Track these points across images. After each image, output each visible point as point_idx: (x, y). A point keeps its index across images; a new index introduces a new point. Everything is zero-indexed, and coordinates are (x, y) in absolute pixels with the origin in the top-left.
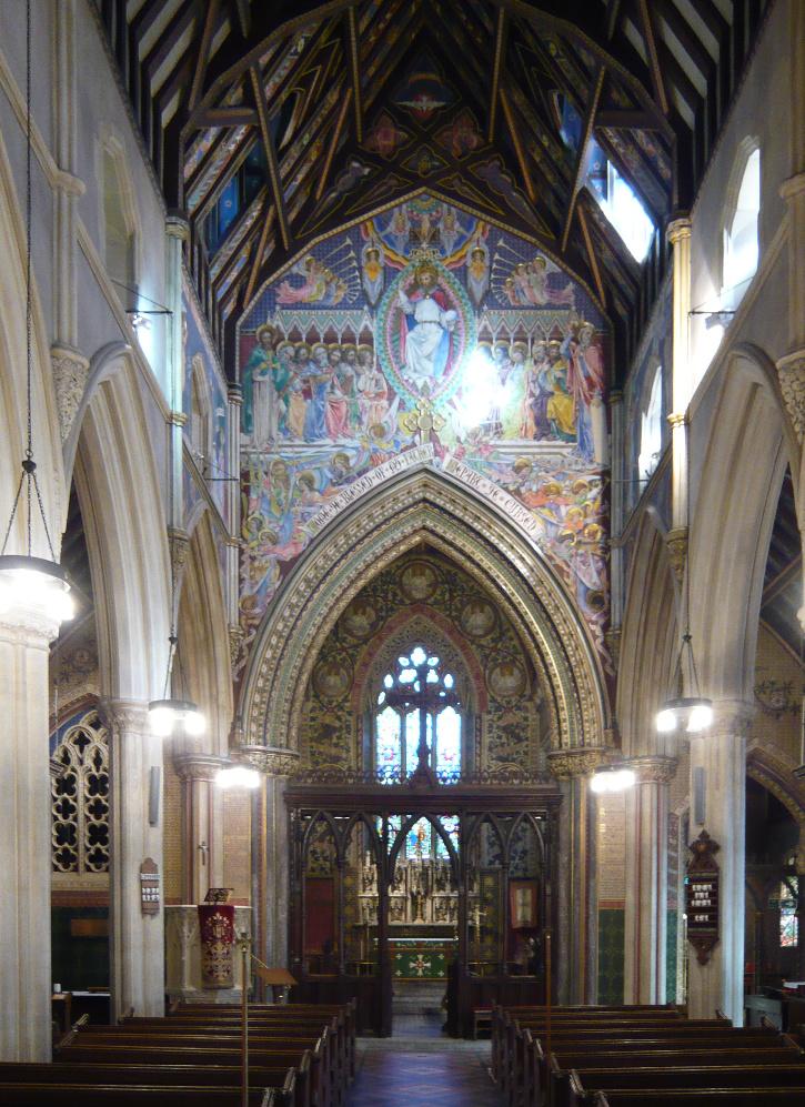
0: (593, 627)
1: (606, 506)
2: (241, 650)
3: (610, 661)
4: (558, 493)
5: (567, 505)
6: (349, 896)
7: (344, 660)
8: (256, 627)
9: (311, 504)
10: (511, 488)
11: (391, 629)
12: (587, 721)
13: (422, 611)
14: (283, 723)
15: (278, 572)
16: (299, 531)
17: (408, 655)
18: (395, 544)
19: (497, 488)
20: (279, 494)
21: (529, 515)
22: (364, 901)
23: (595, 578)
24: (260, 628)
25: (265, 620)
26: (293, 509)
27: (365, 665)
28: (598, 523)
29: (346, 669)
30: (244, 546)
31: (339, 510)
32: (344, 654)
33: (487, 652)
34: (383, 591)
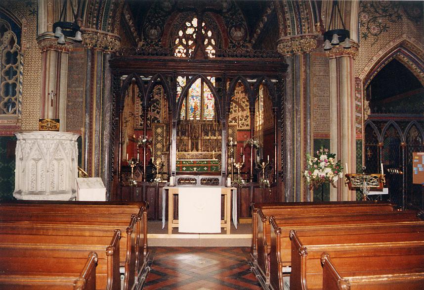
12: (303, 18)
29: (159, 26)
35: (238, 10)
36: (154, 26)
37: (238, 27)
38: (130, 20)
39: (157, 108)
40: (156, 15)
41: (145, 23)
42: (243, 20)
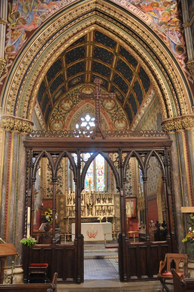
0: (180, 61)
1: (180, 11)
2: (4, 70)
3: (190, 75)
4: (158, 6)
5: (162, 11)
6: (62, 206)
7: (61, 118)
8: (13, 60)
9: (42, 9)
10: (136, 4)
11: (78, 108)
12: (182, 103)
13: (89, 102)
14: (25, 106)
15: (25, 36)
16: (36, 19)
17: (84, 117)
18: (83, 29)
19: (129, 4)
20: (27, 4)
21: (145, 15)
22: (68, 208)
23: (178, 40)
24: (15, 60)
25: (18, 56)
26: (34, 10)
27: (69, 120)
28: (177, 17)
29: (61, 121)
30: (9, 25)
31: (56, 11)
32: (61, 116)
33: (113, 115)
34: (75, 95)
35: (120, 108)
36: (58, 121)
37: (120, 120)
38: (39, 115)
39: (60, 183)
40: (59, 113)
41: (51, 119)
42: (123, 115)
